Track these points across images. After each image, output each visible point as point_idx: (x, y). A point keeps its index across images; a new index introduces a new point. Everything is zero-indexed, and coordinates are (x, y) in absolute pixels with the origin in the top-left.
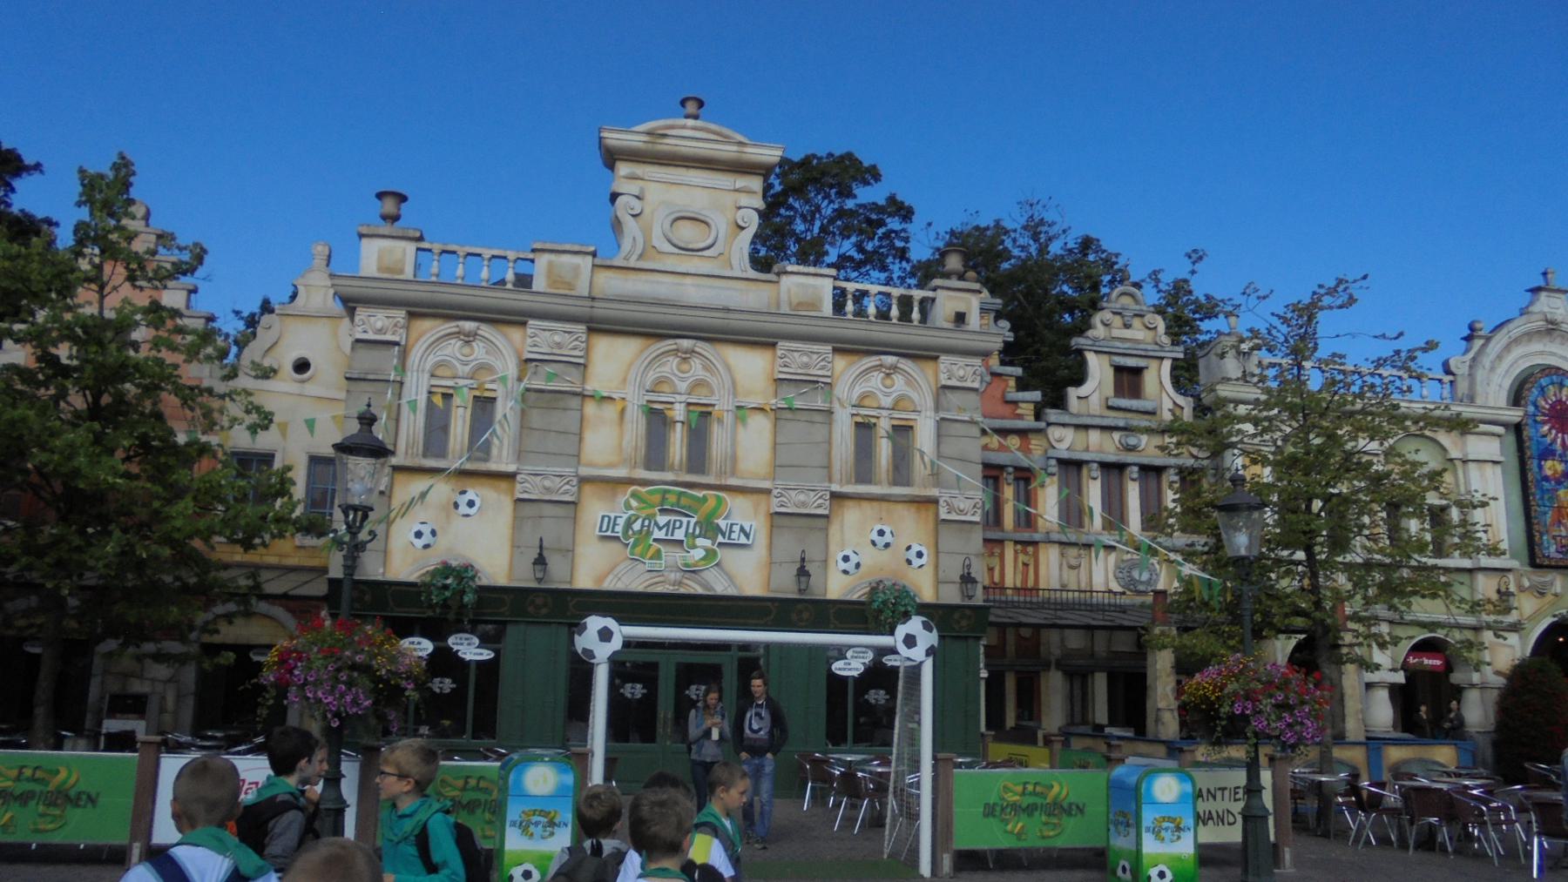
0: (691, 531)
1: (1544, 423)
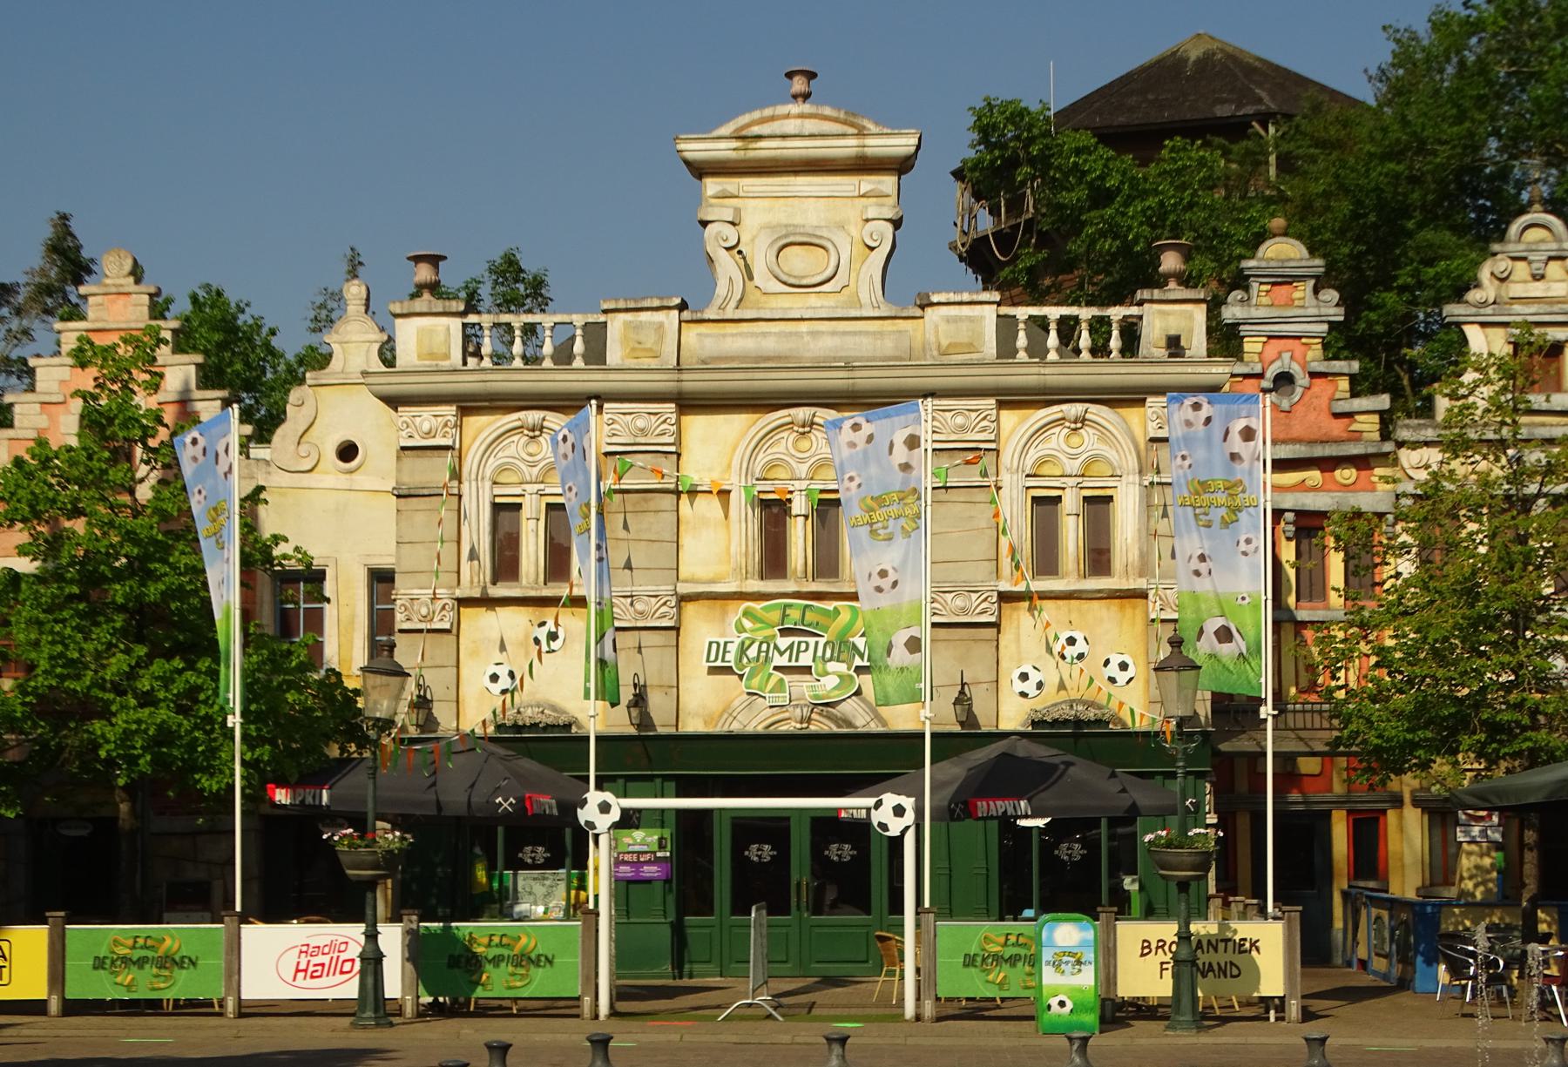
0: (820, 653)
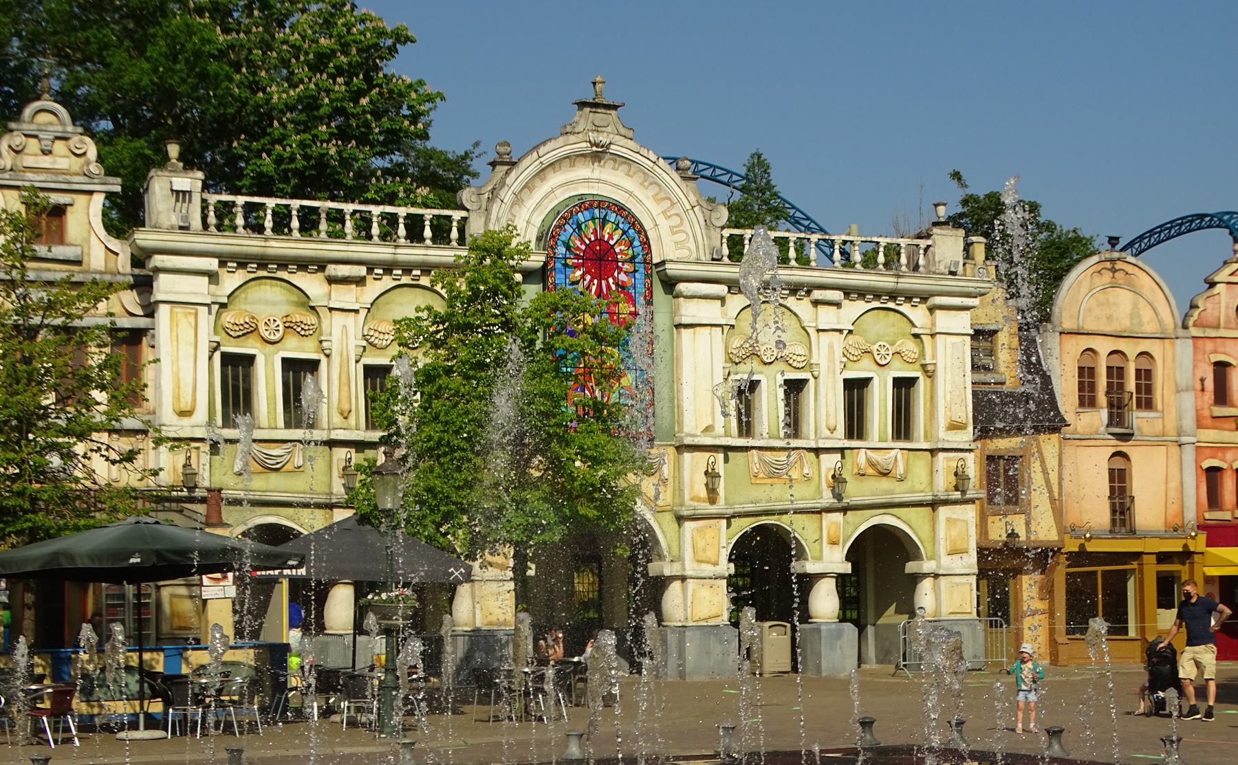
1: (577, 267)
